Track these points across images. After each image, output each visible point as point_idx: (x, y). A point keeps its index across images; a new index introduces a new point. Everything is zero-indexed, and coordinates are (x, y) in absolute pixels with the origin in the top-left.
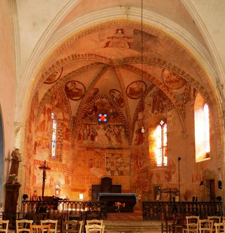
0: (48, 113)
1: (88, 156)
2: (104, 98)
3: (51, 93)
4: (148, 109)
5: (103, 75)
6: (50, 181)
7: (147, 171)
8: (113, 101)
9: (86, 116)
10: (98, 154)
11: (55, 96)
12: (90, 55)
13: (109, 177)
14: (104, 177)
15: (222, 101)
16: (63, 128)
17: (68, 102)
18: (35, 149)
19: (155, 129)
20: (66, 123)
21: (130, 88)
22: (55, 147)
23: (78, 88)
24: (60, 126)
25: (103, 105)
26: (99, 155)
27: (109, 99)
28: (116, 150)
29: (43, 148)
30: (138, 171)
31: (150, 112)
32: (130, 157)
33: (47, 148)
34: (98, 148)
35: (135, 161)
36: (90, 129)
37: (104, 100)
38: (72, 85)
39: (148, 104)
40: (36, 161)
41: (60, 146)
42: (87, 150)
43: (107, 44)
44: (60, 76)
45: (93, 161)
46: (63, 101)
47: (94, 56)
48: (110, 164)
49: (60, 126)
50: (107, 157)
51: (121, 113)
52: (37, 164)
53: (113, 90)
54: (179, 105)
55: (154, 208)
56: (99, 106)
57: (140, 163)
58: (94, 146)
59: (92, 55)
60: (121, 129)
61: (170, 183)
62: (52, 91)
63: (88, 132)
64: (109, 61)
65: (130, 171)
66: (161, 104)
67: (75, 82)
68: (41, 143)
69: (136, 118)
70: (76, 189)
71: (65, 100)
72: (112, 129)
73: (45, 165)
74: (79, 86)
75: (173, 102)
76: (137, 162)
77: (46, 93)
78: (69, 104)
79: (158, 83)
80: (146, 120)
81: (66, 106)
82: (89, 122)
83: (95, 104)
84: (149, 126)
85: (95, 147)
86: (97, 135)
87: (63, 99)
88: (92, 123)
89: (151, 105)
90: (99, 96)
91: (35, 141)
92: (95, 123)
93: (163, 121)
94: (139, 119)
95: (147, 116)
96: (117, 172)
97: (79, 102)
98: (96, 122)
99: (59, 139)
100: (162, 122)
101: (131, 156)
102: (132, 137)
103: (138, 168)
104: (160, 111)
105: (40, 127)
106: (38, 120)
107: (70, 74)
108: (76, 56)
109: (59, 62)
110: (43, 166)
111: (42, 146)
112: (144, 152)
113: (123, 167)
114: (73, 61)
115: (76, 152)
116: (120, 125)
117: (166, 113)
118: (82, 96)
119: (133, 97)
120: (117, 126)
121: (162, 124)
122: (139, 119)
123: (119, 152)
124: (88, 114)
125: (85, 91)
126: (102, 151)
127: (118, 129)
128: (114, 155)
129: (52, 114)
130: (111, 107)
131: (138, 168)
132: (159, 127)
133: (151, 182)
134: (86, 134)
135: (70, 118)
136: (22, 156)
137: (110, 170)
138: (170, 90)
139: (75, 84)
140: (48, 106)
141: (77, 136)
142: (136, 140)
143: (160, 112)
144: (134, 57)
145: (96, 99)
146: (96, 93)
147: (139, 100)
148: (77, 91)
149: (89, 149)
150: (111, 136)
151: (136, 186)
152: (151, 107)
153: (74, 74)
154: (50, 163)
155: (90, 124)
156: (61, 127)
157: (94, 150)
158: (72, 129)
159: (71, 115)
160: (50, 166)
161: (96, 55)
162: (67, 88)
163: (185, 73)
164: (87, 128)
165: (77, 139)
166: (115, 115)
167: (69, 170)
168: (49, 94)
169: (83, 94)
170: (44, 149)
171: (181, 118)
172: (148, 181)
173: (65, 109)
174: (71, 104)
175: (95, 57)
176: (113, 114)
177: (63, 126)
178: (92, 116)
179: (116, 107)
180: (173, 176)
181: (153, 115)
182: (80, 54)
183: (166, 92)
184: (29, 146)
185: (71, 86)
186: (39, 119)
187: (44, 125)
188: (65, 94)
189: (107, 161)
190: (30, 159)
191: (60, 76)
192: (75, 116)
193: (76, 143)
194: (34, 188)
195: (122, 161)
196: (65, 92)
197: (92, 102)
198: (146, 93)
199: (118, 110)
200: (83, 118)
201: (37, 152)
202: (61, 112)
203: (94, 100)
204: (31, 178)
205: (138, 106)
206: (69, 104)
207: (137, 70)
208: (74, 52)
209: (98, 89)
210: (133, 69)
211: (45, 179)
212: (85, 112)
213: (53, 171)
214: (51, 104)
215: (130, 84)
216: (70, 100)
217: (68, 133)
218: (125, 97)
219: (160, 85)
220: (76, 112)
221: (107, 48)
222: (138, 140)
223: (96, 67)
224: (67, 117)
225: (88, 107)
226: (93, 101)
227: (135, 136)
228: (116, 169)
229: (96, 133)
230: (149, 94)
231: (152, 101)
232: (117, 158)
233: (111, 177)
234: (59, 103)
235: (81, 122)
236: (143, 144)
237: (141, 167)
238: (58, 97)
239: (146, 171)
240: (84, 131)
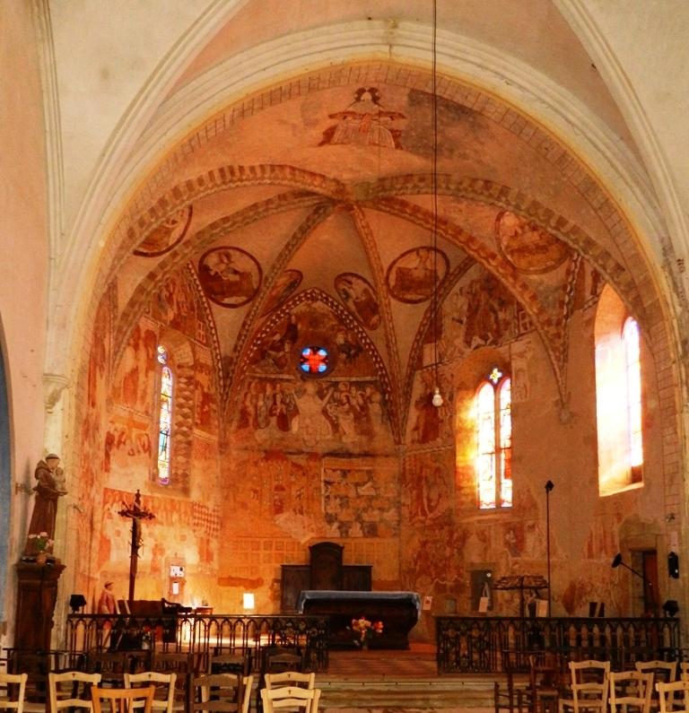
0: (146, 346)
2: (318, 299)
3: (155, 286)
4: (455, 333)
6: (155, 554)
7: (450, 524)
8: (347, 309)
9: (262, 354)
10: (301, 473)
12: (276, 168)
13: (334, 541)
14: (319, 542)
15: (679, 309)
16: (192, 392)
17: (208, 311)
18: (107, 455)
19: (474, 395)
20: (202, 378)
21: (399, 268)
22: (167, 450)
23: (238, 269)
24: (182, 386)
25: (314, 320)
26: (304, 474)
27: (332, 303)
28: (354, 459)
29: (132, 454)
30: (423, 522)
31: (459, 342)
32: (399, 479)
34: (300, 452)
35: (414, 492)
36: (274, 396)
37: (319, 305)
38: (222, 262)
39: (453, 319)
40: (109, 493)
41: (184, 445)
42: (267, 459)
43: (329, 136)
44: (184, 234)
45: (284, 493)
46: (193, 309)
47: (288, 171)
48: (338, 501)
49: (182, 386)
50: (327, 479)
51: (369, 345)
52: (114, 501)
53: (345, 274)
54: (549, 322)
55: (471, 637)
56: (303, 324)
57: (429, 500)
58: (287, 447)
59: (282, 167)
60: (372, 394)
62: (159, 277)
63: (270, 403)
64: (333, 187)
65: (399, 522)
66: (493, 319)
67: (231, 251)
68: (124, 437)
69: (417, 362)
70: (232, 579)
71: (199, 307)
72: (344, 394)
73: (137, 504)
74: (243, 264)
76: (419, 497)
77: (140, 285)
78: (212, 317)
79: (485, 255)
80: (446, 368)
81: (202, 324)
82: (272, 373)
83: (290, 318)
84: (457, 385)
85: (291, 451)
86: (296, 412)
87: (191, 303)
88: (281, 376)
89: (461, 322)
90: (302, 295)
91: (108, 433)
92: (292, 377)
93: (499, 371)
94: (425, 365)
95: (451, 355)
96: (359, 525)
97: (243, 311)
98: (294, 375)
99: (180, 425)
100: (496, 375)
101: (402, 479)
102: (405, 418)
103: (424, 513)
105: (122, 390)
106: (116, 366)
108: (232, 172)
109: (181, 189)
110: (132, 509)
111: (128, 447)
112: (441, 466)
113: (376, 512)
114: (224, 187)
115: (233, 467)
116: (367, 382)
117: (507, 347)
118: (252, 294)
119: (408, 297)
120: (359, 385)
121: (495, 381)
122: (425, 364)
123: (363, 465)
124: (270, 349)
125: (261, 277)
126: (311, 463)
127: (362, 396)
128: (348, 475)
129: (160, 350)
130: (341, 327)
131: (424, 513)
132: (487, 390)
133: (463, 558)
134: (264, 409)
135: (215, 360)
136: (67, 476)
137: (336, 519)
138: (522, 276)
139: (228, 256)
140: (147, 324)
141: (237, 416)
142: (416, 428)
143: (489, 342)
144: (412, 175)
145: (294, 303)
146: (293, 285)
147: (425, 306)
148: (237, 278)
149: (271, 455)
150: (340, 416)
151: (418, 568)
152: (463, 328)
153: (226, 225)
154: (152, 498)
155: (275, 379)
156: (185, 390)
157: (287, 459)
158: (222, 395)
159: (218, 351)
160: (153, 507)
161: (293, 169)
162: (204, 270)
163: (566, 222)
164: (265, 391)
165: (235, 424)
166: (353, 352)
167: (212, 519)
168: (149, 289)
169: (255, 286)
170: (133, 455)
171: (554, 362)
172: (452, 555)
173: (200, 334)
174: (218, 319)
175: (291, 174)
176: (346, 348)
177: (192, 387)
178: (281, 354)
179: (355, 327)
180: (530, 540)
181: (468, 351)
182: (246, 165)
183: (507, 282)
184: (90, 445)
185: (218, 264)
186: (118, 365)
187: (135, 383)
188: (200, 288)
189: (327, 494)
190: (92, 486)
191: (184, 234)
192: (229, 354)
193: (232, 438)
194: (104, 574)
195: (373, 493)
196: (198, 282)
197: (283, 311)
198: (447, 283)
199: (362, 338)
200: (254, 361)
201: (113, 466)
202: (187, 344)
203: (288, 307)
204: (95, 544)
205: (422, 325)
206: (212, 317)
207: (419, 215)
208: (225, 160)
209: (300, 273)
210: (408, 210)
211: (138, 547)
212: (259, 342)
213: (162, 524)
214: (156, 317)
215: (397, 256)
216: (215, 307)
217: (209, 407)
219: (491, 261)
220: (232, 342)
221: (328, 148)
222: (421, 428)
223: (294, 204)
224: (205, 357)
225: (271, 328)
226: (284, 308)
227: (414, 415)
228: (354, 517)
229: (295, 406)
230: (456, 289)
231: (465, 308)
232: (357, 485)
233: (340, 542)
234: (179, 314)
235: (247, 374)
236: (439, 440)
237: (431, 511)
238: (179, 297)
239: (446, 524)
240: (257, 401)
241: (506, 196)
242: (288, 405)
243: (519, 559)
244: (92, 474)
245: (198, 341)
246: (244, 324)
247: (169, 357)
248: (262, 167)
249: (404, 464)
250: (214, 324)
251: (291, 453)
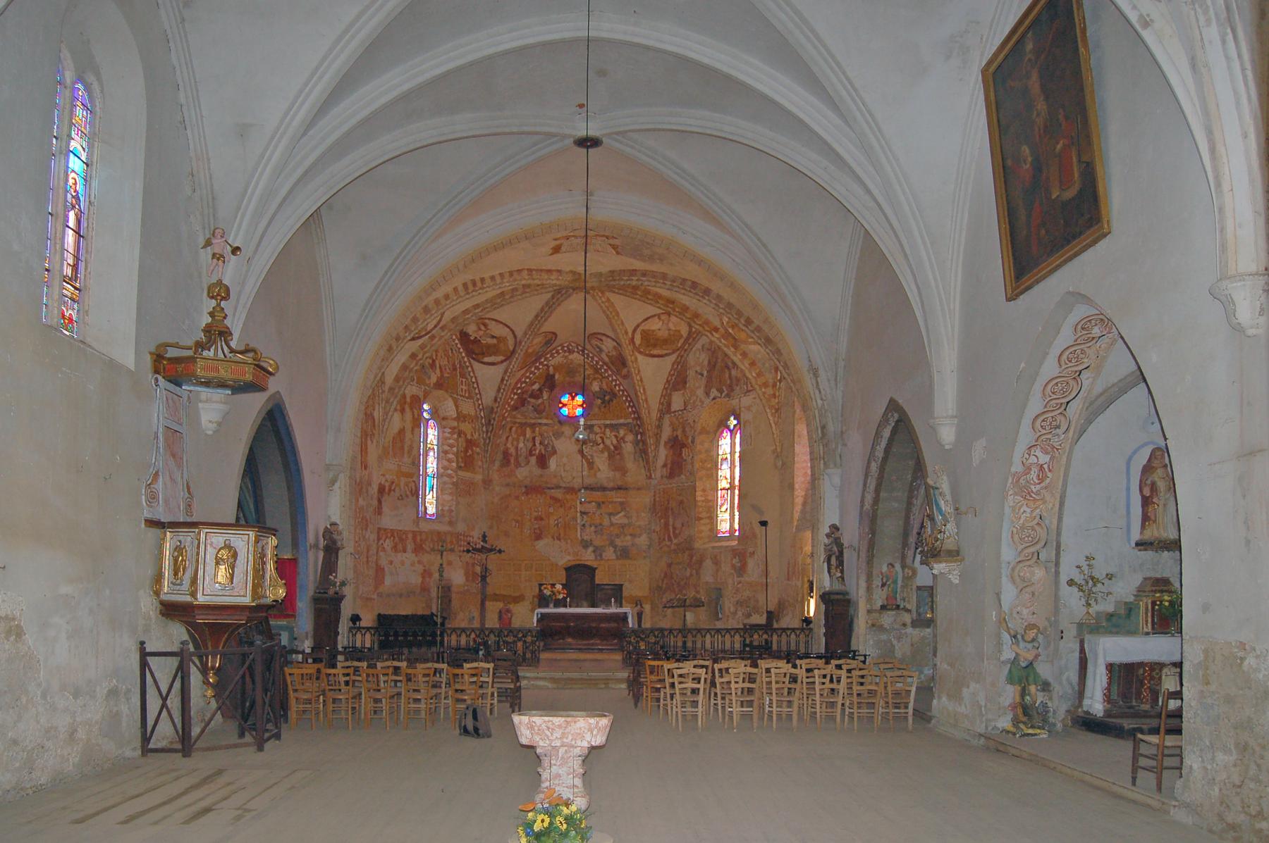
0: (411, 409)
1: (531, 509)
2: (574, 351)
3: (416, 364)
4: (697, 385)
5: (559, 305)
6: (423, 577)
7: (691, 549)
8: (602, 360)
9: (522, 402)
10: (558, 504)
12: (515, 274)
13: (589, 563)
14: (574, 563)
15: (820, 402)
17: (470, 369)
18: (380, 502)
20: (466, 427)
21: (643, 330)
22: (435, 490)
24: (447, 435)
25: (570, 370)
26: (561, 506)
27: (588, 355)
28: (608, 492)
29: (401, 498)
30: (669, 547)
31: (700, 392)
32: (650, 509)
33: (413, 495)
34: (558, 487)
35: (662, 521)
36: (534, 439)
38: (480, 329)
39: (696, 372)
40: (382, 532)
42: (527, 493)
43: (557, 250)
44: (440, 320)
45: (543, 523)
46: (455, 369)
47: (525, 273)
48: (593, 528)
49: (447, 435)
50: (583, 510)
51: (623, 391)
52: (387, 537)
53: (595, 334)
54: (765, 385)
55: (525, 642)
56: (560, 374)
57: (674, 528)
58: (547, 483)
59: (519, 271)
60: (625, 435)
61: (742, 579)
62: (420, 356)
63: (530, 445)
64: (570, 278)
65: (649, 546)
66: (727, 376)
70: (497, 595)
72: (598, 436)
75: (750, 377)
76: (666, 524)
77: (404, 363)
78: (474, 373)
79: (708, 329)
80: (690, 415)
82: (531, 418)
84: (698, 431)
85: (549, 486)
86: (555, 452)
87: (454, 365)
88: (540, 421)
89: (702, 375)
91: (380, 484)
92: (550, 422)
94: (673, 410)
95: (694, 402)
96: (612, 549)
97: (502, 367)
98: (552, 419)
100: (733, 422)
101: (653, 509)
103: (670, 539)
104: (726, 392)
105: (391, 449)
106: (385, 430)
108: (474, 284)
109: (430, 306)
111: (397, 494)
112: (685, 501)
113: (629, 538)
114: (467, 296)
115: (496, 500)
116: (621, 424)
117: (737, 400)
118: (509, 354)
119: (655, 352)
120: (613, 427)
121: (732, 427)
122: (673, 410)
123: (617, 497)
125: (516, 341)
126: (568, 497)
127: (616, 436)
128: (603, 506)
130: (596, 376)
131: (670, 539)
132: (727, 434)
133: (699, 578)
134: (524, 450)
136: (345, 534)
137: (591, 544)
138: (743, 346)
139: (485, 325)
140: (412, 390)
141: (500, 456)
142: (665, 465)
143: (723, 395)
144: (636, 270)
145: (552, 355)
146: (548, 343)
148: (495, 341)
150: (595, 454)
151: (664, 586)
152: (704, 381)
153: (477, 311)
155: (534, 424)
156: (450, 439)
157: (545, 493)
158: (485, 440)
159: (480, 402)
160: (421, 540)
161: (530, 270)
162: (464, 336)
163: (753, 322)
164: (525, 435)
165: (497, 464)
166: (607, 398)
168: (412, 366)
169: (511, 348)
170: (402, 499)
171: (771, 418)
172: (691, 575)
174: (479, 374)
175: (529, 275)
176: (602, 394)
179: (609, 375)
180: (751, 563)
181: (707, 401)
182: (486, 276)
183: (730, 351)
184: (364, 499)
185: (476, 331)
186: (387, 429)
187: (402, 441)
188: (461, 350)
189: (583, 522)
190: (366, 529)
191: (440, 320)
192: (490, 404)
193: (495, 476)
195: (625, 521)
196: (459, 346)
198: (691, 340)
199: (615, 385)
200: (515, 408)
201: (385, 509)
202: (450, 399)
203: (546, 359)
206: (474, 373)
207: (650, 297)
209: (554, 334)
210: (639, 293)
212: (519, 391)
214: (420, 382)
215: (641, 321)
216: (476, 365)
217: (472, 450)
218: (627, 351)
219: (714, 333)
220: (492, 394)
222: (669, 466)
223: (537, 290)
224: (468, 408)
226: (542, 360)
227: (663, 453)
228: (608, 542)
229: (553, 447)
230: (699, 346)
231: (706, 363)
232: (610, 514)
233: (594, 564)
234: (442, 376)
235: (508, 419)
236: (683, 476)
237: (675, 538)
239: (687, 549)
240: (518, 444)
241: (708, 296)
242: (546, 446)
245: (461, 396)
246: (502, 380)
247: (435, 413)
248: (501, 275)
249: (654, 496)
251: (549, 488)
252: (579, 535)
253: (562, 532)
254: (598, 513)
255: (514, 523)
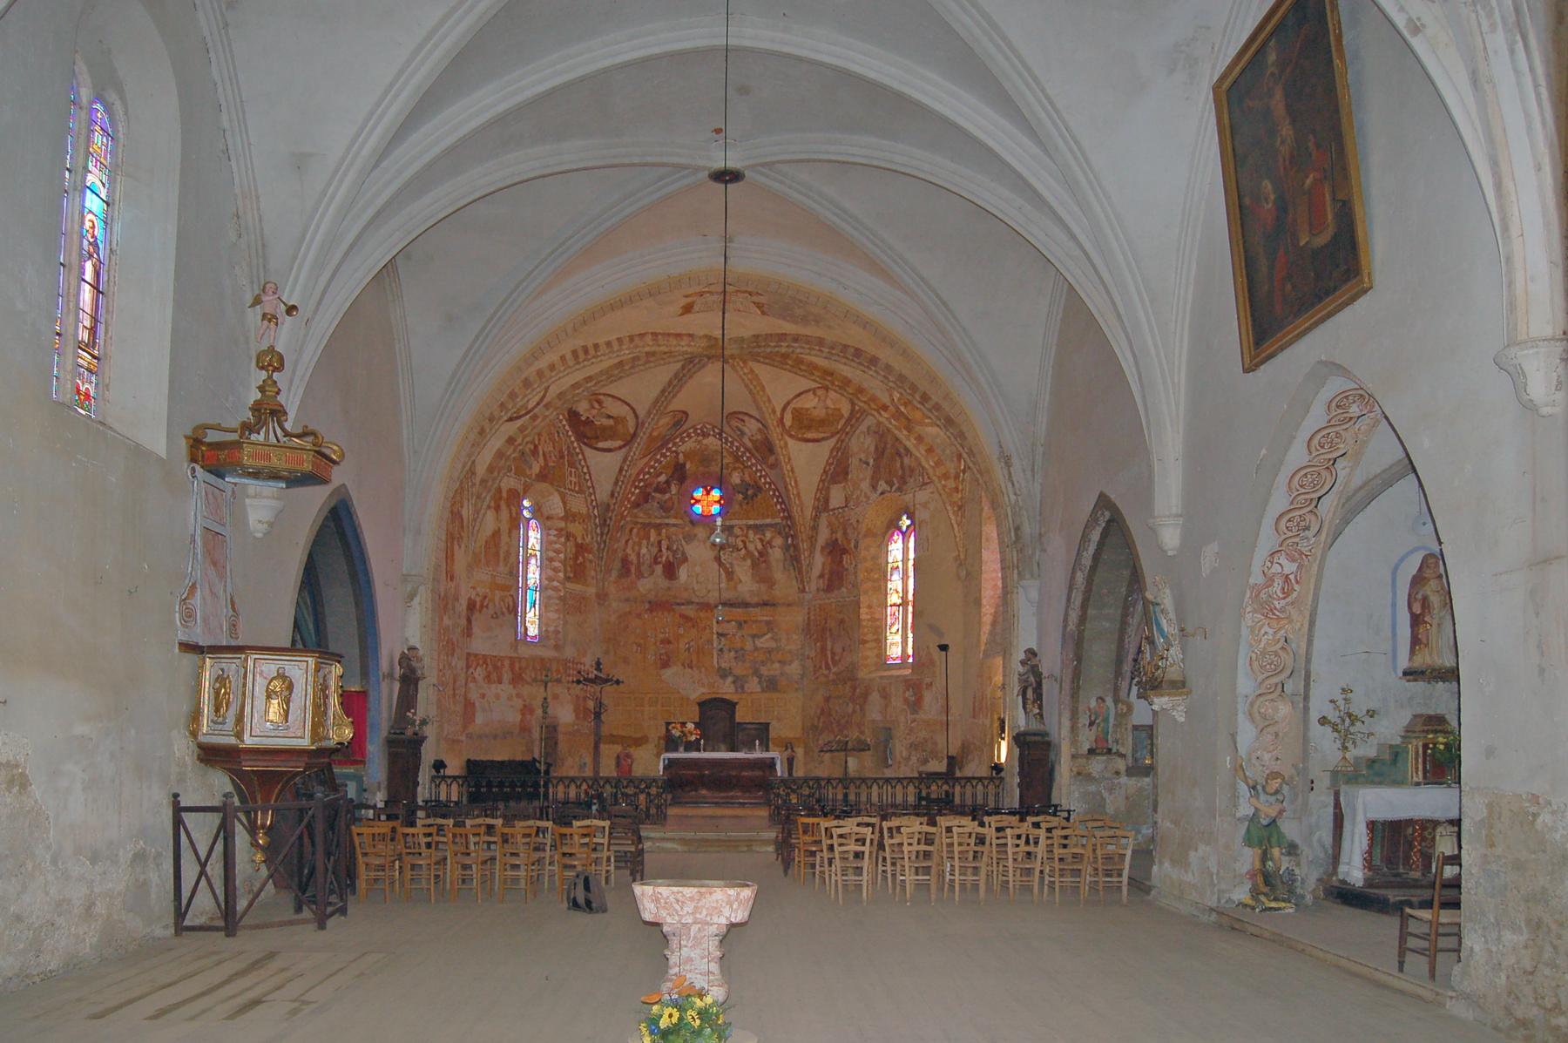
0: (508, 506)
2: (709, 435)
3: (515, 451)
4: (861, 476)
5: (691, 377)
6: (523, 714)
7: (854, 679)
8: (744, 445)
9: (645, 497)
10: (690, 624)
11: (532, 447)
12: (636, 339)
13: (727, 697)
14: (709, 697)
15: (1013, 497)
17: (580, 456)
18: (469, 621)
20: (576, 528)
21: (794, 409)
22: (537, 606)
24: (552, 538)
25: (705, 458)
26: (693, 626)
27: (726, 439)
28: (751, 609)
29: (495, 616)
30: (826, 676)
31: (865, 485)
32: (803, 630)
34: (690, 603)
35: (818, 644)
36: (660, 543)
38: (593, 407)
39: (860, 460)
40: (472, 658)
42: (651, 610)
43: (688, 309)
44: (544, 396)
45: (671, 646)
46: (562, 457)
47: (649, 338)
48: (733, 654)
49: (552, 538)
50: (720, 631)
51: (770, 484)
52: (478, 665)
53: (735, 413)
54: (946, 476)
55: (648, 794)
56: (692, 463)
57: (833, 654)
58: (675, 597)
59: (642, 335)
60: (772, 538)
62: (519, 441)
63: (655, 550)
64: (704, 343)
65: (802, 676)
66: (898, 465)
70: (614, 736)
72: (739, 539)
75: (927, 466)
76: (824, 649)
77: (499, 449)
78: (585, 462)
79: (875, 407)
80: (852, 513)
82: (656, 517)
84: (862, 533)
85: (678, 601)
86: (685, 559)
87: (561, 451)
88: (667, 521)
89: (868, 464)
91: (470, 599)
92: (680, 522)
94: (831, 507)
95: (858, 498)
96: (756, 680)
97: (620, 455)
98: (682, 519)
99: (550, 579)
100: (905, 522)
101: (807, 629)
103: (828, 667)
105: (483, 555)
106: (475, 532)
107: (575, 386)
108: (586, 351)
109: (532, 379)
111: (491, 611)
112: (847, 619)
113: (777, 665)
114: (578, 367)
115: (613, 619)
116: (767, 525)
117: (911, 495)
118: (629, 438)
119: (810, 435)
120: (758, 529)
121: (904, 529)
122: (831, 507)
123: (762, 615)
125: (637, 422)
126: (702, 614)
127: (761, 540)
128: (745, 626)
130: (737, 465)
131: (828, 667)
132: (898, 538)
133: (864, 715)
134: (647, 556)
136: (427, 661)
137: (730, 673)
138: (918, 429)
140: (509, 482)
141: (617, 565)
142: (822, 576)
143: (894, 488)
144: (786, 334)
145: (682, 440)
146: (677, 424)
148: (611, 422)
150: (735, 562)
151: (821, 725)
152: (869, 472)
153: (589, 385)
155: (660, 525)
156: (556, 543)
157: (673, 610)
158: (599, 544)
159: (593, 497)
160: (520, 669)
161: (655, 334)
162: (573, 416)
163: (930, 398)
164: (649, 538)
165: (614, 574)
166: (750, 492)
168: (508, 453)
169: (632, 431)
170: (497, 618)
171: (953, 517)
172: (854, 712)
174: (591, 462)
176: (744, 488)
179: (752, 464)
180: (928, 697)
181: (874, 496)
182: (601, 341)
183: (902, 435)
184: (450, 618)
185: (588, 410)
186: (478, 531)
187: (497, 546)
188: (570, 433)
189: (720, 646)
190: (453, 655)
191: (544, 396)
192: (606, 500)
193: (612, 589)
195: (773, 645)
196: (567, 428)
198: (854, 421)
199: (760, 477)
200: (637, 505)
201: (476, 630)
202: (556, 494)
203: (675, 444)
206: (585, 462)
207: (803, 367)
209: (685, 413)
210: (790, 362)
212: (642, 484)
214: (519, 472)
215: (791, 397)
216: (588, 452)
217: (583, 557)
219: (882, 413)
220: (608, 487)
222: (827, 576)
223: (663, 359)
224: (578, 504)
226: (670, 445)
227: (819, 560)
228: (751, 671)
229: (684, 553)
230: (863, 428)
231: (872, 449)
232: (754, 636)
233: (734, 698)
234: (546, 465)
235: (628, 519)
236: (844, 589)
237: (835, 665)
239: (849, 679)
240: (640, 549)
241: (875, 366)
242: (675, 552)
243: (917, 716)
244: (453, 644)
246: (621, 470)
249: (809, 613)
250: (588, 467)
251: (678, 604)
252: (715, 663)
253: (694, 658)
254: (739, 634)
255: (635, 648)
